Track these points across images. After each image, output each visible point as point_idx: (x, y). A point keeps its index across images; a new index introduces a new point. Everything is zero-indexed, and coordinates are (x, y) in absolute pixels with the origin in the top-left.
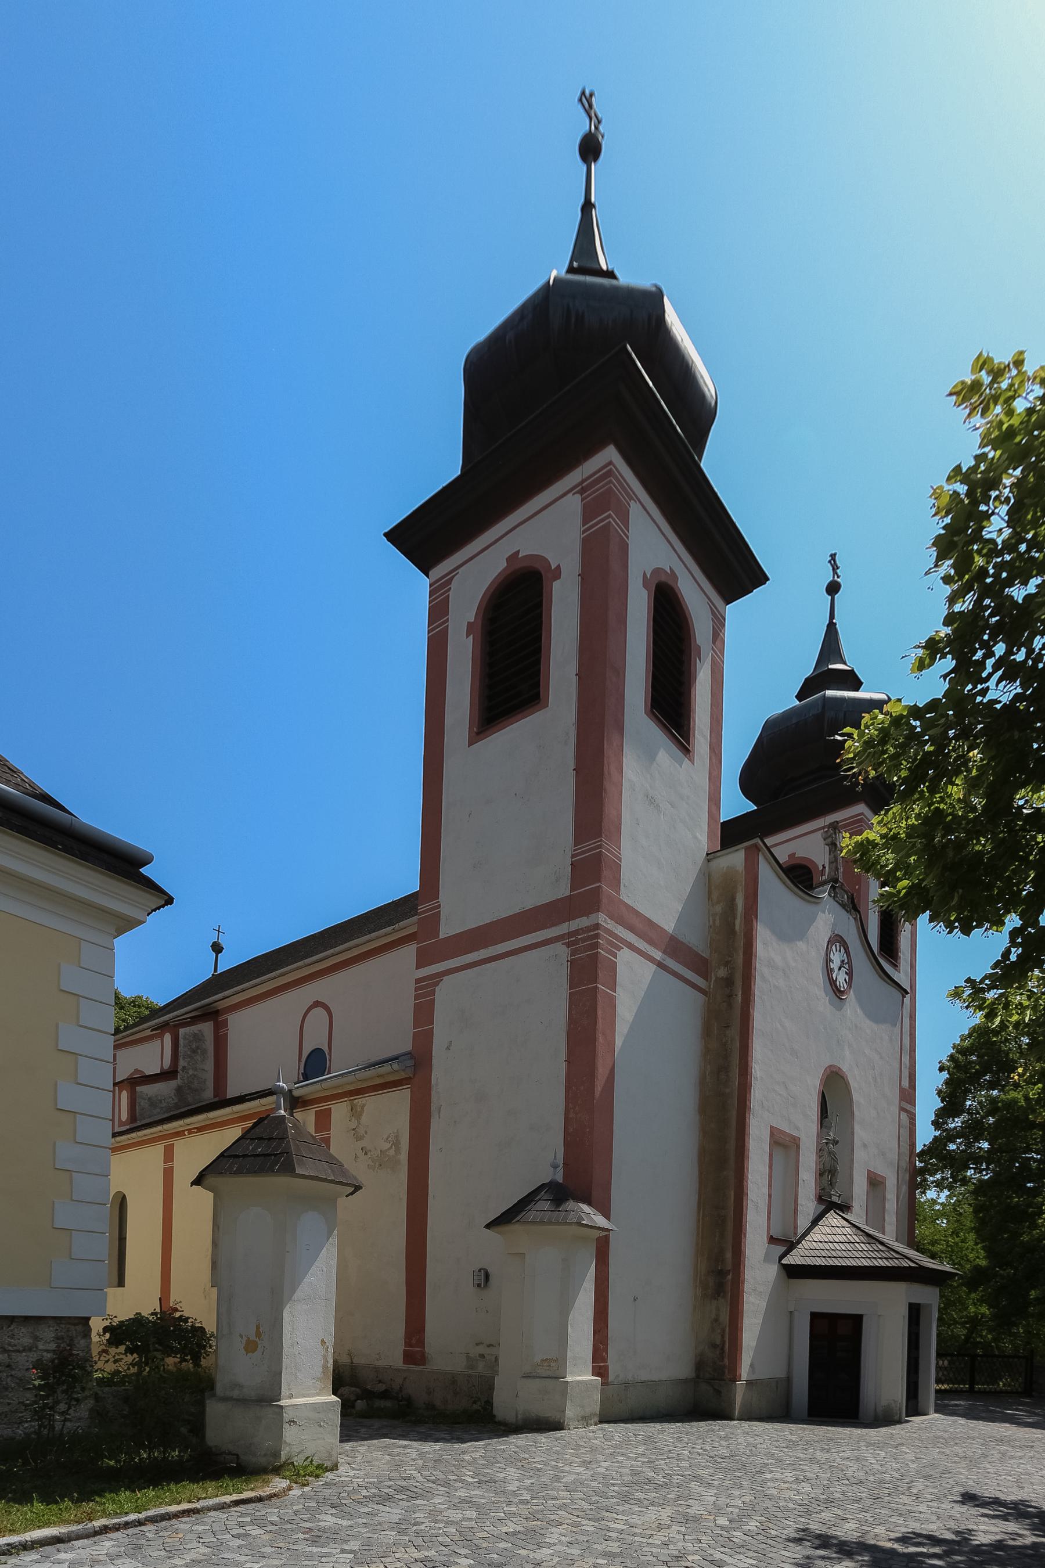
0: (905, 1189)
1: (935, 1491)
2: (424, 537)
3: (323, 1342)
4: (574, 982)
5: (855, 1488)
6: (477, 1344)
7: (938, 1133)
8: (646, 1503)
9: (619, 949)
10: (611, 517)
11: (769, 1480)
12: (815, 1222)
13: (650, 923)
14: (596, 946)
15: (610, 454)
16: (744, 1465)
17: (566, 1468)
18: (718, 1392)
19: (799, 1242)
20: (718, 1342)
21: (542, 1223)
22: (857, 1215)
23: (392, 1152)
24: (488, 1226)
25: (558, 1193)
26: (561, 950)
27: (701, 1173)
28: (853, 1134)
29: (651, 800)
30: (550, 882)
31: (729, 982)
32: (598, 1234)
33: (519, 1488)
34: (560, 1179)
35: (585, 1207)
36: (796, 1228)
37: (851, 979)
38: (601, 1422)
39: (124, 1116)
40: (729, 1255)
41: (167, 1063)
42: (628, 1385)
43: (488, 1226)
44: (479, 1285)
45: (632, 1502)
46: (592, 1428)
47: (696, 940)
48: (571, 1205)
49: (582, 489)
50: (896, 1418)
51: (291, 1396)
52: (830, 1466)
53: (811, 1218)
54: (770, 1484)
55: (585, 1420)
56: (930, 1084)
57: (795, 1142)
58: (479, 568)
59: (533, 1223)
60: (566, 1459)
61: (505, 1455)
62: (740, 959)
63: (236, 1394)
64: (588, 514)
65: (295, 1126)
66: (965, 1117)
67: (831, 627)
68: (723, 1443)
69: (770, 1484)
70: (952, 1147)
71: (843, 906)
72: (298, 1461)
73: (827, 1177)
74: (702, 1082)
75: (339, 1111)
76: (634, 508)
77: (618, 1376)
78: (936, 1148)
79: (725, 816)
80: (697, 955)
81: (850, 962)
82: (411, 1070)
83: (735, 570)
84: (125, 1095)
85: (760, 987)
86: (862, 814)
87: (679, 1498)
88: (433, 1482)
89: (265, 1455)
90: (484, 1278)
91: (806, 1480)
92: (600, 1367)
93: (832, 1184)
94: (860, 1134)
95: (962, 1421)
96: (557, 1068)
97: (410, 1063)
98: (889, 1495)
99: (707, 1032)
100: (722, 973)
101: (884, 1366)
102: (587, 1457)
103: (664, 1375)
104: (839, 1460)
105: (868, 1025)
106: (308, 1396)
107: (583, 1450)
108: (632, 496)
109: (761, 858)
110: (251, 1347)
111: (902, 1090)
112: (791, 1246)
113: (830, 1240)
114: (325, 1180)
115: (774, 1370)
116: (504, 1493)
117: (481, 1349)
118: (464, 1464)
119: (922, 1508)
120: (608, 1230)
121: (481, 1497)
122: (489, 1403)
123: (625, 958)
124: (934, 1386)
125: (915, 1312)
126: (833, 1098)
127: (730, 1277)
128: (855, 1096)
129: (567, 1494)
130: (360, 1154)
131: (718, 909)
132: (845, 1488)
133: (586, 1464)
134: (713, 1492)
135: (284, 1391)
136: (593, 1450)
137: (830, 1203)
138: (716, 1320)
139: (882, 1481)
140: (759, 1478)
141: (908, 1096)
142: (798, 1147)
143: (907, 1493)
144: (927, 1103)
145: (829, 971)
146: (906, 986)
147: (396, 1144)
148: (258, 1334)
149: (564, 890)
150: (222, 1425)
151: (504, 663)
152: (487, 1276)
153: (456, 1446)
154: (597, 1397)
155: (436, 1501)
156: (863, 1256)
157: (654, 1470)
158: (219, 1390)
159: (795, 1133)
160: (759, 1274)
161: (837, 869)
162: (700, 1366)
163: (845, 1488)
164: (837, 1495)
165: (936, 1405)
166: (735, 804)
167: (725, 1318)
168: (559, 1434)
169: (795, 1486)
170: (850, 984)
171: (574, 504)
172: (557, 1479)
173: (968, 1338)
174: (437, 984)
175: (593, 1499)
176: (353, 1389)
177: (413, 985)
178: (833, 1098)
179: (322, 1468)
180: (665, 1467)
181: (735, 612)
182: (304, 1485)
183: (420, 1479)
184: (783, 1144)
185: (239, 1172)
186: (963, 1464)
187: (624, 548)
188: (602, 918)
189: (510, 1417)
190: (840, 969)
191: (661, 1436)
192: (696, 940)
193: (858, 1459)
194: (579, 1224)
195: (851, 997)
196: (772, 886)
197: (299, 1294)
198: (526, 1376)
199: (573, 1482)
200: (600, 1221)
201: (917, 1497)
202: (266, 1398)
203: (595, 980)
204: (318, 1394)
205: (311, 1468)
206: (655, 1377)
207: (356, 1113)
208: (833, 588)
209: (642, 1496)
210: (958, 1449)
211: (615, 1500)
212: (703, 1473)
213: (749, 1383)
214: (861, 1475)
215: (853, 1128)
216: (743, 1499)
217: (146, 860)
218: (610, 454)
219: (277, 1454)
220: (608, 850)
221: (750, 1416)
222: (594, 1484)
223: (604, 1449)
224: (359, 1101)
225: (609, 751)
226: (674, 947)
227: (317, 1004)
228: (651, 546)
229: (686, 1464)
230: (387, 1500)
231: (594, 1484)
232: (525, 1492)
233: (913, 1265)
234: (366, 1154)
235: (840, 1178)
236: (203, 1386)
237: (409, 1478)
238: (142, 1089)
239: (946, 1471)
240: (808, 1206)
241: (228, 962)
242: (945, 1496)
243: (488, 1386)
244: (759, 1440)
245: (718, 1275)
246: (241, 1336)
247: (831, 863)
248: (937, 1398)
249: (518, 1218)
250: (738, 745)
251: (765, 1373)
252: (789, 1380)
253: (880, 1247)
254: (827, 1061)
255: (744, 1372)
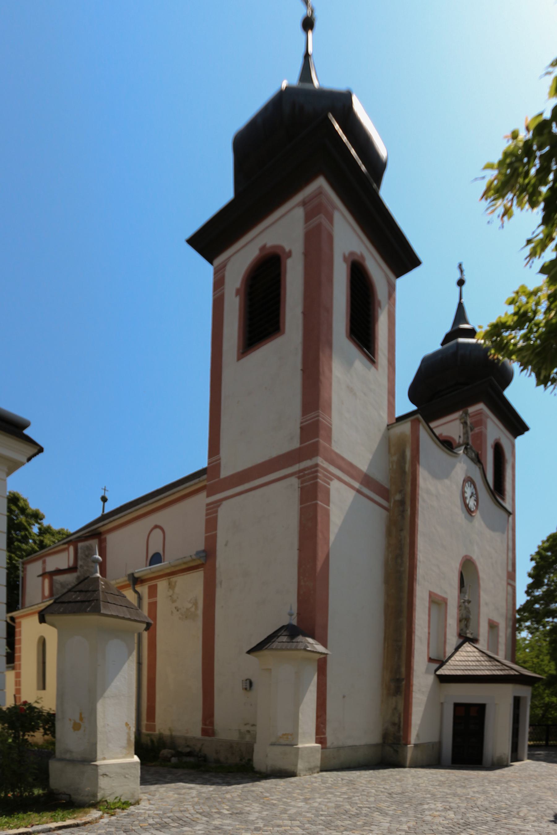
0: (510, 630)
1: (535, 814)
2: (210, 241)
3: (127, 724)
4: (302, 501)
5: (483, 813)
6: (246, 724)
7: (529, 598)
8: (342, 829)
9: (331, 480)
10: (322, 218)
11: (426, 809)
12: (457, 649)
13: (351, 465)
14: (316, 477)
15: (321, 182)
16: (410, 799)
17: (293, 803)
18: (396, 751)
19: (447, 661)
20: (397, 721)
21: (281, 649)
22: (483, 644)
23: (193, 609)
24: (249, 652)
25: (292, 632)
26: (294, 481)
27: (386, 619)
28: (479, 596)
29: (351, 390)
30: (287, 440)
31: (402, 503)
32: (318, 656)
33: (257, 818)
34: (295, 622)
35: (310, 640)
36: (445, 653)
37: (477, 503)
38: (322, 771)
39: (47, 593)
40: (403, 670)
41: (71, 563)
42: (339, 748)
43: (249, 652)
44: (246, 689)
45: (333, 828)
46: (316, 775)
47: (381, 476)
48: (300, 638)
49: (304, 203)
50: (505, 763)
51: (104, 759)
52: (466, 798)
53: (454, 647)
54: (427, 813)
55: (311, 770)
56: (524, 567)
57: (444, 601)
58: (243, 256)
59: (276, 649)
60: (294, 797)
61: (254, 794)
62: (408, 488)
63: (68, 756)
64: (308, 217)
65: (106, 584)
66: (545, 588)
67: (461, 307)
68: (398, 783)
69: (427, 813)
70: (537, 606)
71: (472, 460)
72: (110, 799)
73: (464, 623)
74: (386, 564)
75: (162, 585)
76: (337, 216)
77: (333, 743)
78: (527, 607)
79: (399, 413)
80: (382, 486)
81: (476, 494)
82: (206, 560)
83: (402, 257)
84: (47, 582)
85: (421, 505)
86: (481, 409)
87: (365, 824)
88: (200, 813)
89: (87, 796)
90: (249, 685)
91: (451, 808)
92: (321, 738)
93: (467, 626)
94: (484, 597)
95: (544, 764)
96: (293, 555)
97: (204, 554)
98: (506, 818)
99: (389, 533)
100: (398, 497)
101: (498, 733)
102: (308, 796)
103: (363, 742)
104: (471, 794)
105: (488, 533)
106: (117, 758)
107: (306, 791)
108: (335, 207)
109: (421, 428)
110: (76, 727)
111: (508, 573)
112: (442, 663)
113: (467, 659)
114: (123, 618)
115: (431, 737)
116: (246, 821)
117: (248, 728)
118: (225, 801)
119: (529, 827)
120: (327, 654)
121: (229, 825)
122: (251, 760)
123: (335, 487)
124: (527, 743)
125: (517, 701)
126: (467, 576)
127: (404, 683)
128: (481, 574)
129: (288, 823)
130: (174, 611)
131: (395, 458)
132: (476, 814)
133: (306, 800)
134: (388, 819)
135: (99, 755)
136: (313, 790)
137: (466, 638)
138: (395, 709)
139: (500, 808)
140: (420, 808)
141: (511, 576)
142: (446, 604)
143: (517, 816)
144: (523, 581)
145: (464, 499)
146: (510, 510)
147: (196, 604)
148: (81, 719)
149: (296, 444)
150: (60, 776)
151: (258, 311)
152: (251, 684)
153: (224, 788)
154: (319, 756)
155: (198, 828)
156: (486, 669)
157: (352, 804)
158: (58, 754)
159: (444, 596)
160: (422, 680)
161: (468, 438)
162: (385, 736)
163: (476, 814)
164: (472, 820)
165: (528, 755)
166: (404, 405)
167: (401, 707)
168: (293, 779)
169: (443, 814)
170: (477, 506)
171: (300, 212)
172: (285, 811)
173: (543, 715)
174: (219, 506)
175: (307, 826)
176: (170, 751)
177: (204, 508)
178: (467, 576)
179: (126, 804)
180: (358, 802)
181: (402, 283)
182: (112, 815)
183: (192, 811)
184: (438, 602)
185: (64, 613)
186: (549, 793)
187: (331, 238)
188: (320, 460)
189: (263, 769)
190: (471, 497)
191: (358, 780)
192: (381, 476)
193: (484, 792)
194: (305, 649)
195: (477, 515)
196: (428, 447)
197: (108, 693)
198: (273, 744)
199: (295, 813)
200: (320, 648)
201: (524, 819)
202: (88, 759)
203: (316, 498)
204: (124, 757)
205: (118, 805)
206: (357, 743)
207: (171, 586)
208: (461, 283)
209: (339, 823)
210: (544, 783)
211: (321, 827)
212: (383, 805)
213: (416, 746)
214: (486, 804)
215: (479, 593)
216: (409, 824)
217: (25, 425)
218: (321, 182)
219: (95, 795)
220: (323, 419)
221: (416, 765)
222: (309, 815)
223: (320, 789)
224: (174, 579)
225: (323, 358)
226: (367, 480)
227: (156, 527)
228: (347, 238)
229: (372, 799)
230: (164, 827)
231: (309, 815)
232: (260, 821)
233: (517, 673)
234: (178, 611)
235: (472, 624)
236: (48, 753)
237: (185, 811)
238: (58, 578)
239: (540, 799)
240: (452, 639)
241: (110, 507)
242: (542, 817)
243: (250, 749)
244: (421, 781)
245: (397, 682)
246: (70, 720)
247: (464, 434)
248: (529, 750)
249: (266, 647)
250: (406, 372)
251: (424, 740)
252: (440, 743)
253: (497, 663)
254: (463, 553)
255: (413, 739)
